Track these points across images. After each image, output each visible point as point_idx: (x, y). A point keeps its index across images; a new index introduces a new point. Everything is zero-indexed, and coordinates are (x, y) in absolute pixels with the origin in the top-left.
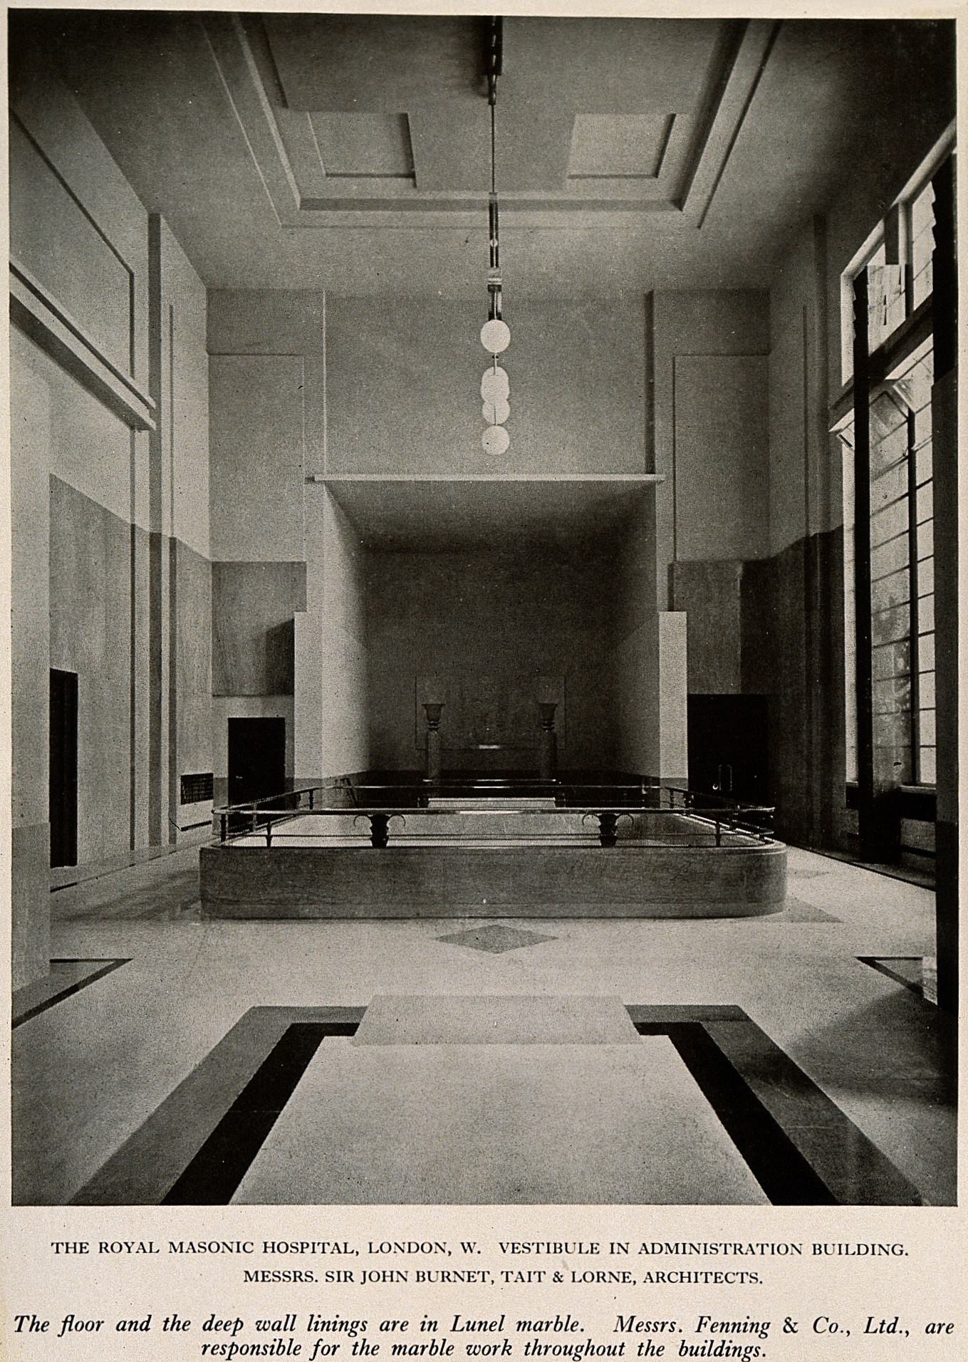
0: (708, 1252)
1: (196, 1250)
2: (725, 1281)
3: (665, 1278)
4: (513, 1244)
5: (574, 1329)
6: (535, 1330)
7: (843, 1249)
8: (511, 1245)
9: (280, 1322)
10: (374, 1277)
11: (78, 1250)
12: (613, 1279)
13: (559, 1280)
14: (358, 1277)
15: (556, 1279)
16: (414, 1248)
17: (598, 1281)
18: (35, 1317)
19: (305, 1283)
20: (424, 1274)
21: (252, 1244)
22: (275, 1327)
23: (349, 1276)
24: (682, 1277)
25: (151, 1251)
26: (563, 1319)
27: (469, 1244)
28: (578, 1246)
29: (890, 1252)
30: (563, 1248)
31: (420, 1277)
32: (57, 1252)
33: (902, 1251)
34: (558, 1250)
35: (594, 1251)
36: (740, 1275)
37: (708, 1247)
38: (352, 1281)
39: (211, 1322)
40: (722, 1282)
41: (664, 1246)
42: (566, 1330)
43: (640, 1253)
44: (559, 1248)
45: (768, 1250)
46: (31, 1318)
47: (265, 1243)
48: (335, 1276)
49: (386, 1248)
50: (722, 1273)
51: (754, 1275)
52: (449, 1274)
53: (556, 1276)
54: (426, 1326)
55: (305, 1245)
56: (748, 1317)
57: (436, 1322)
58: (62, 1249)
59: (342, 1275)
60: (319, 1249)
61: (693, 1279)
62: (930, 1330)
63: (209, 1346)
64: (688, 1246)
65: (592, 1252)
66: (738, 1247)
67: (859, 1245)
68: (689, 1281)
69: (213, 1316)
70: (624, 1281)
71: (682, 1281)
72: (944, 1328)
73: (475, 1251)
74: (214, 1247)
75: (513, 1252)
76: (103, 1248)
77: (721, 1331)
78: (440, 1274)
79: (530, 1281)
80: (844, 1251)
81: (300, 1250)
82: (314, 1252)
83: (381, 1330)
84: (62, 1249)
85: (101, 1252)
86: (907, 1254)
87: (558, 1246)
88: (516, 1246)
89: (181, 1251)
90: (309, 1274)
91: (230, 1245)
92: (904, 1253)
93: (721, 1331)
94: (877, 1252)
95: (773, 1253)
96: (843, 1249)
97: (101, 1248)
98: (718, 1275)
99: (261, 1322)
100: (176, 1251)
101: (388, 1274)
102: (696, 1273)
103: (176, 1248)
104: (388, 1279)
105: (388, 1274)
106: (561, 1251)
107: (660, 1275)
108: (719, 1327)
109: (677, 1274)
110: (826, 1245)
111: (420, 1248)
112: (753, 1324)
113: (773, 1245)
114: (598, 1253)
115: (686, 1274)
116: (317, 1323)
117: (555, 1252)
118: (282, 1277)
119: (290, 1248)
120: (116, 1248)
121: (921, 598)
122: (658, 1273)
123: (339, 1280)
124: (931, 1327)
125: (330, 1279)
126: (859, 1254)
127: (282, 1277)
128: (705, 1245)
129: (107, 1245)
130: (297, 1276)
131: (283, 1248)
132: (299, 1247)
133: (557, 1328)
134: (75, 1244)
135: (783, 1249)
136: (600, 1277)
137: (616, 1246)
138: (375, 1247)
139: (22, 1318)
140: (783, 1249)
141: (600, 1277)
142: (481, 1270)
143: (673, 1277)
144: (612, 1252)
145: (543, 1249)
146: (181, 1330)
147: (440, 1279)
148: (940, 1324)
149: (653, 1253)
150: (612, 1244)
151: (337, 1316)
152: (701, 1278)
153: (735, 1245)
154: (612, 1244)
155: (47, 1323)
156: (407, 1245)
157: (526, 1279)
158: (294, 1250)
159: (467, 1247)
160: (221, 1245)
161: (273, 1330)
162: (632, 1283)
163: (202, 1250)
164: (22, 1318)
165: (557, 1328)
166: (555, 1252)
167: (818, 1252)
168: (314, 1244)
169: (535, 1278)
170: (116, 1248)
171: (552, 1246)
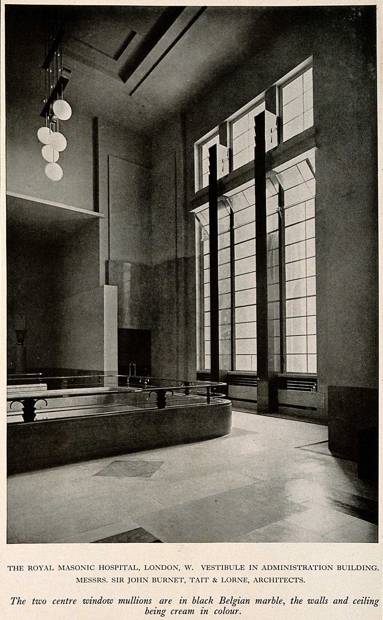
0: (292, 569)
1: (70, 569)
2: (289, 582)
3: (263, 580)
4: (207, 566)
5: (280, 602)
6: (98, 603)
7: (350, 568)
8: (206, 566)
9: (318, 600)
10: (134, 580)
12: (239, 581)
13: (215, 581)
14: (126, 580)
15: (214, 581)
16: (164, 568)
17: (233, 582)
18: (19, 598)
19: (102, 583)
20: (156, 579)
22: (316, 602)
23: (122, 580)
25: (50, 570)
26: (276, 599)
27: (188, 566)
28: (235, 566)
29: (371, 569)
30: (229, 567)
31: (154, 580)
32: (10, 570)
33: (376, 569)
34: (227, 568)
35: (242, 569)
36: (295, 579)
37: (292, 567)
38: (123, 582)
39: (101, 600)
41: (273, 567)
42: (277, 603)
43: (263, 570)
44: (227, 567)
45: (318, 568)
46: (18, 598)
47: (100, 566)
48: (116, 580)
49: (152, 568)
51: (301, 579)
53: (214, 580)
54: (182, 601)
55: (117, 567)
58: (12, 569)
60: (123, 568)
61: (275, 581)
62: (335, 602)
64: (283, 567)
65: (241, 569)
66: (305, 567)
67: (357, 566)
69: (102, 597)
70: (175, 582)
72: (72, 602)
73: (191, 569)
74: (77, 568)
76: (30, 568)
77: (61, 603)
78: (163, 579)
79: (202, 582)
80: (351, 568)
81: (115, 569)
83: (334, 603)
84: (12, 569)
85: (29, 570)
86: (378, 570)
87: (227, 566)
88: (85, 579)
89: (64, 570)
91: (84, 567)
92: (377, 569)
93: (61, 603)
94: (365, 569)
95: (320, 569)
96: (350, 568)
98: (286, 579)
99: (85, 600)
100: (276, 569)
101: (139, 579)
102: (276, 578)
103: (61, 568)
104: (139, 581)
105: (139, 579)
106: (341, 569)
107: (261, 579)
108: (61, 602)
111: (167, 568)
112: (94, 600)
113: (320, 566)
114: (244, 569)
115: (272, 579)
116: (368, 600)
117: (225, 569)
119: (110, 568)
120: (36, 568)
121: (228, 247)
122: (260, 578)
123: (117, 582)
124: (317, 601)
125: (114, 581)
126: (357, 570)
128: (291, 566)
130: (99, 580)
131: (107, 568)
133: (273, 602)
134: (18, 566)
135: (324, 568)
136: (234, 580)
137: (252, 567)
139: (14, 598)
140: (324, 568)
141: (234, 580)
142: (295, 577)
143: (266, 580)
144: (250, 569)
145: (220, 568)
146: (279, 603)
147: (163, 581)
149: (268, 569)
150: (250, 566)
151: (92, 597)
152: (279, 580)
153: (304, 566)
154: (250, 566)
155: (301, 600)
156: (161, 566)
157: (200, 581)
158: (112, 569)
159: (188, 567)
160: (155, 567)
161: (315, 603)
162: (248, 582)
163: (73, 569)
164: (14, 598)
165: (273, 602)
166: (225, 569)
167: (339, 569)
168: (121, 566)
169: (204, 580)
170: (36, 568)
171: (224, 567)
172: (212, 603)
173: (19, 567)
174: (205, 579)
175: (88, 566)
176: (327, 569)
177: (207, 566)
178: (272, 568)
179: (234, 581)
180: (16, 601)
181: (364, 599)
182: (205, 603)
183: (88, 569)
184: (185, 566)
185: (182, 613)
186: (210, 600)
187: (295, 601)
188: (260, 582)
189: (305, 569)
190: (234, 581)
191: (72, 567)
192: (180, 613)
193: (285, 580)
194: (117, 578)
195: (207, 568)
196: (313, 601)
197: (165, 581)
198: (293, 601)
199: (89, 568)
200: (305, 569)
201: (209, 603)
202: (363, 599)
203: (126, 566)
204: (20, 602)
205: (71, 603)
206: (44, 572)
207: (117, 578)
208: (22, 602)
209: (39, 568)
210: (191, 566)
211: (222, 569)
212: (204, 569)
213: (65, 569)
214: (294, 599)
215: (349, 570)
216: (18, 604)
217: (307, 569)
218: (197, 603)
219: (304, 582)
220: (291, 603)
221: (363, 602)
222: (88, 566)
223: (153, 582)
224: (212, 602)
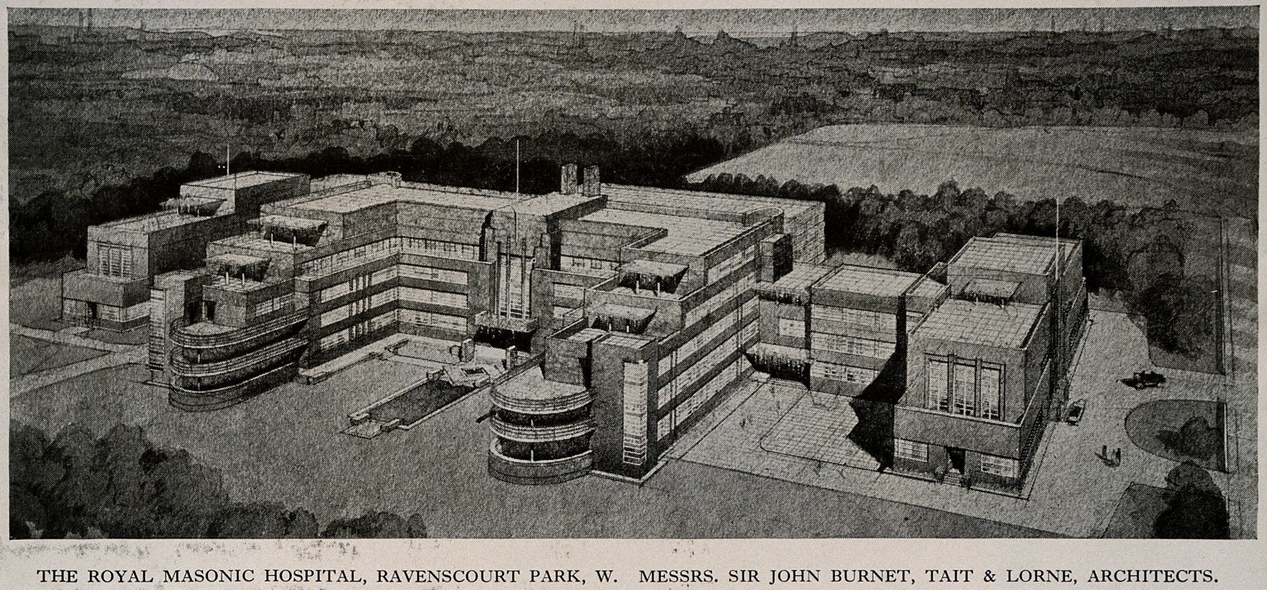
1: (193, 579)
2: (1176, 580)
8: (415, 573)
11: (656, 579)
13: (991, 579)
15: (988, 578)
20: (840, 573)
21: (252, 572)
24: (1130, 576)
36: (1192, 573)
40: (1173, 581)
43: (1090, 581)
47: (267, 571)
48: (740, 575)
50: (1173, 572)
51: (1207, 573)
52: (867, 573)
53: (988, 575)
55: (309, 573)
58: (49, 577)
59: (747, 574)
60: (324, 577)
68: (1138, 580)
71: (1129, 580)
75: (418, 581)
78: (858, 573)
81: (304, 579)
82: (319, 580)
84: (49, 577)
85: (91, 581)
88: (662, 574)
89: (177, 581)
90: (708, 573)
97: (380, 576)
102: (1145, 572)
107: (1107, 573)
109: (1124, 572)
114: (76, 581)
118: (680, 577)
119: (293, 576)
120: (107, 576)
123: (743, 580)
127: (680, 577)
132: (304, 575)
134: (63, 571)
138: (1014, 576)
143: (1120, 576)
152: (1151, 577)
157: (952, 578)
163: (200, 579)
167: (837, 578)
168: (319, 571)
169: (961, 577)
170: (107, 576)
173: (66, 574)
175: (238, 571)
184: (598, 572)
188: (1104, 580)
189: (382, 579)
194: (743, 571)
203: (332, 573)
207: (743, 571)
209: (116, 577)
210: (611, 571)
212: (409, 580)
219: (1216, 581)
222: (238, 571)
223: (834, 580)
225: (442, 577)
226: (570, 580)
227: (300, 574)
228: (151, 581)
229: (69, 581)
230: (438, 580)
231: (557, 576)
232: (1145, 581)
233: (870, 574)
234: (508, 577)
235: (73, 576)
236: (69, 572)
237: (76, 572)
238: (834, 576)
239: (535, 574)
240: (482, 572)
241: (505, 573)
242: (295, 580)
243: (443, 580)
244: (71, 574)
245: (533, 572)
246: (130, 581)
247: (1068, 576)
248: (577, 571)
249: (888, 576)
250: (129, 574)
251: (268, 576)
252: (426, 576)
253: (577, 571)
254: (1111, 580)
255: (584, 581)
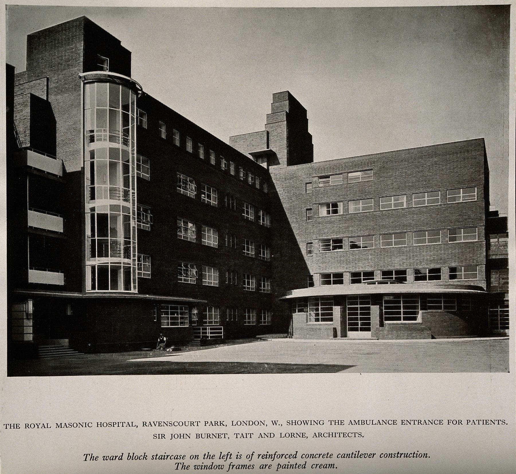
1: (68, 427)
3: (322, 435)
4: (159, 422)
8: (158, 423)
12: (298, 436)
16: (251, 423)
20: (199, 435)
21: (92, 423)
23: (163, 436)
26: (131, 455)
27: (275, 421)
29: (318, 424)
34: (363, 423)
38: (165, 438)
47: (98, 423)
48: (158, 436)
50: (488, 420)
55: (115, 423)
56: (238, 453)
57: (198, 456)
58: (8, 427)
59: (160, 435)
60: (121, 425)
63: (267, 465)
66: (420, 421)
74: (75, 425)
75: (159, 426)
76: (27, 426)
79: (246, 437)
81: (113, 426)
84: (333, 423)
85: (143, 426)
88: (487, 421)
89: (61, 427)
94: (84, 424)
97: (26, 426)
100: (356, 424)
102: (335, 433)
107: (320, 434)
110: (366, 421)
117: (362, 424)
120: (32, 426)
123: (159, 438)
129: (28, 425)
132: (112, 424)
138: (234, 423)
143: (390, 422)
147: (206, 437)
148: (116, 456)
152: (337, 435)
153: (418, 420)
157: (245, 436)
159: (274, 423)
168: (118, 423)
169: (249, 436)
170: (32, 426)
172: (146, 459)
174: (339, 434)
175: (86, 423)
176: (242, 424)
177: (159, 422)
178: (77, 425)
179: (293, 436)
180: (89, 457)
181: (357, 453)
182: (315, 458)
183: (86, 427)
184: (272, 421)
185: (323, 468)
186: (144, 456)
187: (208, 456)
189: (419, 423)
190: (293, 436)
191: (70, 424)
192: (321, 467)
193: (344, 435)
194: (159, 435)
195: (159, 424)
196: (108, 457)
197: (163, 437)
198: (206, 457)
199: (341, 423)
200: (419, 423)
201: (143, 459)
202: (356, 453)
204: (93, 458)
205: (283, 457)
206: (42, 430)
207: (159, 435)
208: (94, 458)
209: (36, 426)
210: (277, 421)
211: (483, 424)
212: (155, 425)
213: (62, 426)
214: (207, 454)
215: (311, 424)
216: (90, 460)
217: (146, 426)
218: (132, 459)
220: (204, 459)
221: (356, 455)
222: (86, 423)
223: (197, 438)
224: (146, 458)
225: (168, 424)
226: (220, 425)
227: (69, 426)
228: (50, 427)
229: (341, 424)
230: (167, 425)
231: (215, 424)
232: (335, 437)
233: (211, 435)
234: (195, 424)
235: (395, 422)
236: (486, 420)
237: (442, 420)
238: (197, 436)
239: (206, 423)
240: (185, 422)
241: (194, 422)
242: (169, 426)
243: (169, 426)
244: (160, 423)
245: (205, 422)
246: (42, 428)
247: (343, 423)
248: (223, 421)
249: (219, 436)
250: (41, 425)
251: (98, 425)
252: (162, 424)
253: (223, 421)
254: (322, 437)
255: (226, 425)
